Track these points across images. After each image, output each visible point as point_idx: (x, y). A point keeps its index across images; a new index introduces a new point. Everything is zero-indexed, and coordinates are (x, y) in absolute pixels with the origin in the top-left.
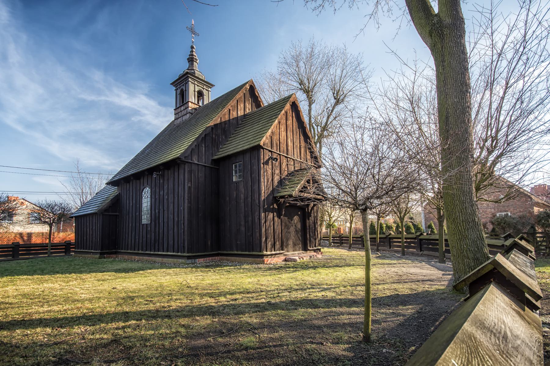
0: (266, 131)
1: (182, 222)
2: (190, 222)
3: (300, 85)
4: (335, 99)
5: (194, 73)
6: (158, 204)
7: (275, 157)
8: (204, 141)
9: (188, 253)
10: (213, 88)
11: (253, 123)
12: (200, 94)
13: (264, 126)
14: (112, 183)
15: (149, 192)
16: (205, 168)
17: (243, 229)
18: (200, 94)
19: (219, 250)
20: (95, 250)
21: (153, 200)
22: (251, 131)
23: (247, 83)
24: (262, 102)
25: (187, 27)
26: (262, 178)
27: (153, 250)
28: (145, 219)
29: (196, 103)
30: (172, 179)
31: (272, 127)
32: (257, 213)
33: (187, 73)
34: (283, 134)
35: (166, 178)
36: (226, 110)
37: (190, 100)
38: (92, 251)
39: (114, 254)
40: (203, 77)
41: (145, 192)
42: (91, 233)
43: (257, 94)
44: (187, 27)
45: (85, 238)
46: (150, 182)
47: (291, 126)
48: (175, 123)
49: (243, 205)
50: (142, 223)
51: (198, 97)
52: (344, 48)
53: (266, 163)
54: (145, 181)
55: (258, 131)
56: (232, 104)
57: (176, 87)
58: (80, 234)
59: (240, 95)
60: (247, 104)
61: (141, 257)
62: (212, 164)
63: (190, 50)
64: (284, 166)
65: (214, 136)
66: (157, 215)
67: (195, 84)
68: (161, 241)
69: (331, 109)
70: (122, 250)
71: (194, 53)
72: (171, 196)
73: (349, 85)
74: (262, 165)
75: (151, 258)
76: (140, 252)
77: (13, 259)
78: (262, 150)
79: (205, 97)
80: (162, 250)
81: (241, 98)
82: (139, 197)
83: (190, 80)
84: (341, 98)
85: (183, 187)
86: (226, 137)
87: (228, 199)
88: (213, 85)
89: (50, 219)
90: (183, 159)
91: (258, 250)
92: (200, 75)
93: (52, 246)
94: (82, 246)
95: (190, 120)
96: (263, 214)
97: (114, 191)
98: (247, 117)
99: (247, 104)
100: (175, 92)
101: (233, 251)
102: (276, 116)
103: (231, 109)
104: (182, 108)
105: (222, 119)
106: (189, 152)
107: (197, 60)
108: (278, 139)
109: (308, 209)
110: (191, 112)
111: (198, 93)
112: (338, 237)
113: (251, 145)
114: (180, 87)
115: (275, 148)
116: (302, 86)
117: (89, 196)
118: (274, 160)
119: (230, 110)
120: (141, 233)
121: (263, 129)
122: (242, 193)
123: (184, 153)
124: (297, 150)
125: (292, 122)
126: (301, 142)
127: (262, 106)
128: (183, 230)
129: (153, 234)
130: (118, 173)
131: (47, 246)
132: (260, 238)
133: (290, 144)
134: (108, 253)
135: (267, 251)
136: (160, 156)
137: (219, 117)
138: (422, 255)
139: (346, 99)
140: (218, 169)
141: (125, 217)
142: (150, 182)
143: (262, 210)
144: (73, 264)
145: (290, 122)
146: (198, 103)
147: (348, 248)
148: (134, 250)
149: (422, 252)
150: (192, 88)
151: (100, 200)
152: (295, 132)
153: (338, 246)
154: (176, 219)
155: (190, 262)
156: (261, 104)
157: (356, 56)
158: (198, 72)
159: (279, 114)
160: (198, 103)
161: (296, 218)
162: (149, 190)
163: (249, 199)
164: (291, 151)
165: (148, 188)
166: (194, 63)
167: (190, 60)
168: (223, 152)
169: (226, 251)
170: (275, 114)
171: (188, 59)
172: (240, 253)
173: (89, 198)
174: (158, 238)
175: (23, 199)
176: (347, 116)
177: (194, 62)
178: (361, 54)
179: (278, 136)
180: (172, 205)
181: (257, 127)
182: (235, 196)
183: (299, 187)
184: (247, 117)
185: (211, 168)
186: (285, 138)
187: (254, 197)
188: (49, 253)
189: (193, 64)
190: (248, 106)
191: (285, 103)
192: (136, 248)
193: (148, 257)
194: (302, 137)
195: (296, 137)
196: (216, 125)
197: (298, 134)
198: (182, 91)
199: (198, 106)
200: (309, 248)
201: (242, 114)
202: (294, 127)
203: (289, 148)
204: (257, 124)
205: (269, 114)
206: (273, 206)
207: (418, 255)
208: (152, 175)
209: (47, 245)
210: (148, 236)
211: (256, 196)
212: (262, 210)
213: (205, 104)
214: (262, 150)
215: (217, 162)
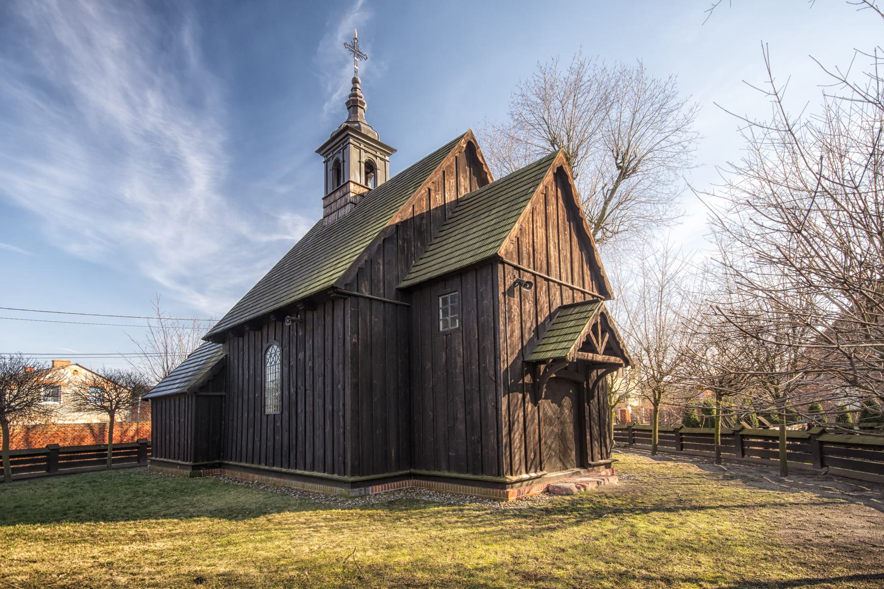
0: (508, 227)
1: (341, 413)
2: (356, 413)
3: (553, 145)
4: (619, 167)
5: (360, 127)
6: (294, 376)
7: (525, 279)
8: (382, 252)
9: (352, 475)
10: (394, 155)
11: (478, 214)
12: (370, 168)
13: (503, 218)
14: (213, 337)
15: (278, 354)
16: (384, 307)
17: (462, 427)
18: (370, 168)
19: (411, 465)
20: (184, 460)
21: (286, 369)
22: (474, 230)
23: (462, 137)
24: (490, 174)
25: (345, 44)
26: (501, 323)
27: (287, 465)
28: (272, 405)
29: (363, 183)
30: (321, 328)
31: (521, 218)
32: (491, 396)
33: (347, 128)
34: (540, 232)
35: (309, 328)
36: (423, 191)
37: (352, 178)
38: (180, 462)
39: (217, 468)
40: (375, 135)
41: (271, 354)
42: (177, 429)
43: (480, 159)
44: (345, 44)
45: (168, 437)
46: (279, 337)
47: (555, 217)
48: (324, 224)
49: (460, 379)
50: (266, 413)
51: (367, 173)
52: (640, 70)
53: (510, 292)
54: (272, 332)
55: (489, 229)
56: (435, 179)
57: (327, 156)
58: (159, 428)
59: (449, 160)
60: (462, 179)
61: (264, 477)
62: (397, 298)
63: (352, 86)
64: (543, 299)
65: (400, 242)
66: (294, 398)
67: (360, 149)
68: (300, 449)
69: (611, 187)
70: (231, 460)
71: (358, 92)
72: (319, 361)
73: (646, 140)
74: (501, 296)
75: (282, 480)
76: (263, 467)
77: (48, 474)
78: (500, 266)
79: (380, 173)
80: (302, 467)
81: (450, 166)
82: (259, 363)
83: (351, 140)
84: (632, 165)
85: (341, 344)
86: (423, 244)
87: (429, 366)
88: (393, 150)
89: (111, 401)
90: (343, 289)
91: (495, 471)
92: (369, 131)
93: (114, 449)
94: (164, 453)
95: (352, 215)
96: (504, 401)
97: (218, 351)
98: (460, 204)
99: (462, 179)
100: (323, 165)
101: (439, 470)
102: (527, 196)
103: (432, 188)
104: (338, 195)
105: (416, 209)
106: (354, 274)
107: (363, 104)
108: (531, 243)
109: (588, 385)
110: (353, 200)
111: (366, 166)
112: (626, 429)
113: (478, 258)
114: (333, 157)
115: (525, 261)
116: (556, 146)
117: (177, 358)
118: (525, 286)
119: (429, 190)
120: (264, 431)
121: (502, 224)
122: (459, 355)
123: (344, 277)
124: (566, 265)
125: (557, 209)
126: (574, 248)
127: (491, 181)
128: (342, 430)
129: (286, 435)
130: (223, 319)
131: (107, 450)
132: (498, 447)
133: (553, 252)
134: (206, 467)
135: (512, 475)
136: (298, 284)
137: (410, 204)
138: (828, 477)
139: (641, 168)
140: (408, 307)
141: (236, 400)
142: (279, 332)
143: (501, 390)
144: (141, 492)
145: (552, 208)
146: (366, 184)
147: (650, 453)
148: (253, 463)
149: (825, 469)
150: (356, 157)
151: (193, 367)
152: (561, 229)
153: (625, 447)
154: (329, 407)
155: (358, 494)
156: (489, 177)
157: (663, 83)
158: (366, 127)
159: (533, 192)
160: (366, 184)
161: (567, 402)
162: (278, 350)
163: (475, 367)
164: (556, 267)
165: (275, 347)
166: (359, 109)
167: (351, 104)
168: (418, 274)
169: (427, 470)
170: (524, 193)
171: (347, 103)
172: (454, 475)
173: (178, 362)
174: (294, 442)
175: (77, 364)
176: (643, 199)
177: (359, 108)
178: (673, 77)
179: (531, 236)
180: (321, 379)
181: (486, 220)
182: (444, 360)
183: (580, 339)
184: (460, 204)
185: (397, 305)
186: (544, 241)
187: (485, 362)
188: (108, 462)
189: (356, 112)
190: (464, 183)
191: (543, 170)
192: (256, 459)
193: (278, 477)
194: (575, 239)
195: (565, 237)
196: (404, 224)
197: (567, 233)
198: (337, 161)
199: (367, 190)
200: (590, 462)
201: (453, 199)
202: (560, 218)
203: (552, 261)
204: (486, 214)
205: (509, 195)
206: (523, 381)
207: (814, 475)
208: (283, 321)
209: (105, 448)
210: (277, 438)
211: (490, 360)
212: (501, 390)
213: (379, 184)
214: (500, 266)
215: (407, 292)
